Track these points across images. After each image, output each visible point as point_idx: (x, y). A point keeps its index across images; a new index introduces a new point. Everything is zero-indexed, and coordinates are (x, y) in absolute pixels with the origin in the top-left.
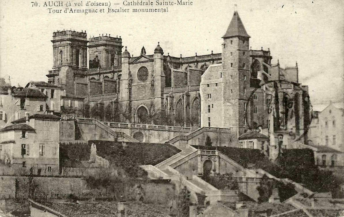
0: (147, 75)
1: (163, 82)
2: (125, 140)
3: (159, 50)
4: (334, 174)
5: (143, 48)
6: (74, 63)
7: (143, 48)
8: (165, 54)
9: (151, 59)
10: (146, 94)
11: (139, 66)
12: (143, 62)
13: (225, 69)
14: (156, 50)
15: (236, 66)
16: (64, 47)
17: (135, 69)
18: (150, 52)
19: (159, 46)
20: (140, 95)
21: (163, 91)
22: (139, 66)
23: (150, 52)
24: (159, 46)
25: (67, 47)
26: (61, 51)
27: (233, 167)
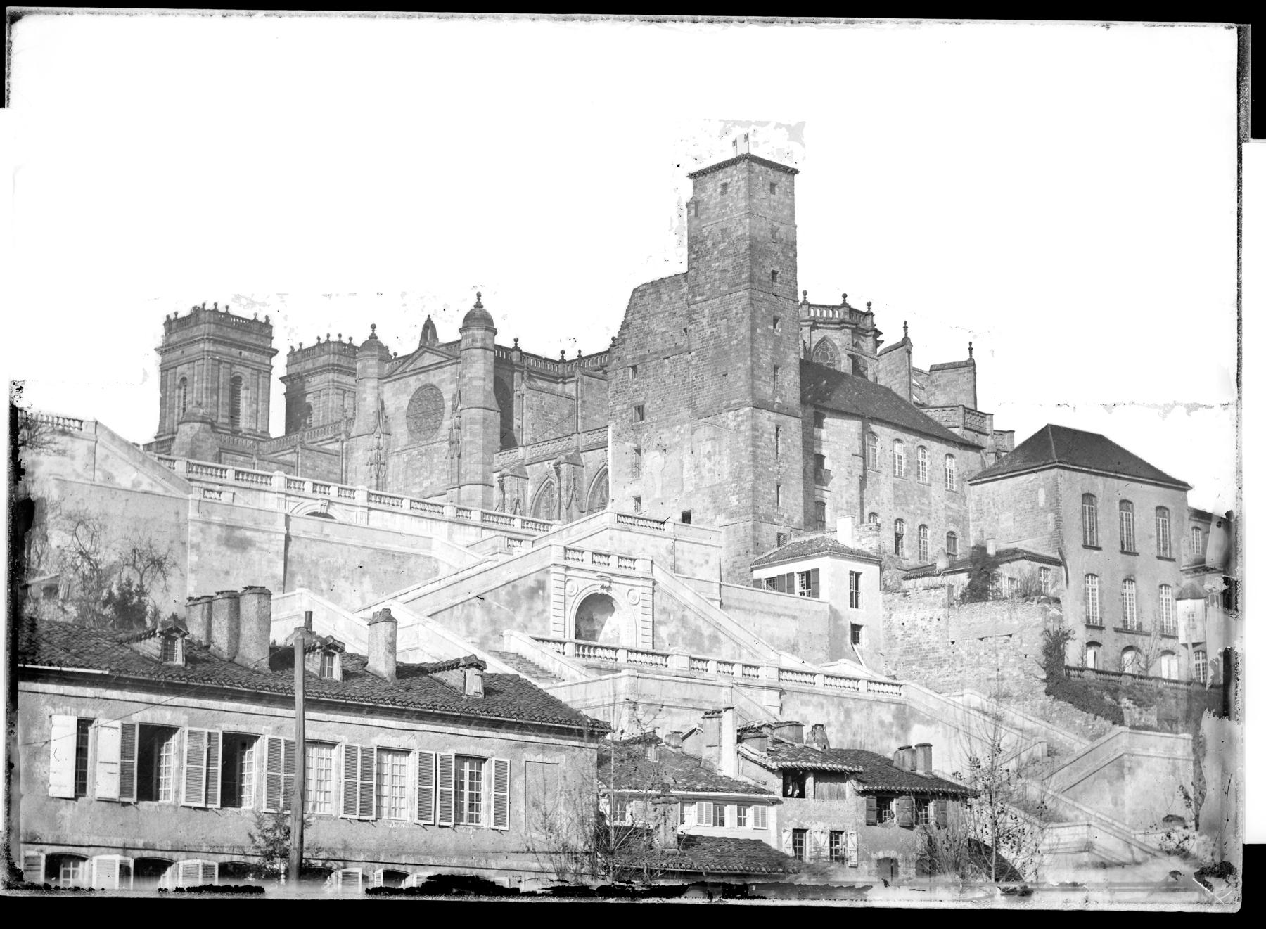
0: (439, 410)
1: (490, 431)
2: (1182, 735)
3: (478, 319)
4: (1044, 677)
5: (429, 321)
6: (223, 416)
7: (429, 321)
8: (504, 340)
9: (453, 352)
10: (434, 480)
11: (414, 383)
12: (425, 369)
13: (698, 299)
14: (468, 318)
15: (744, 276)
16: (191, 365)
17: (398, 398)
18: (448, 332)
19: (479, 306)
20: (415, 484)
21: (490, 464)
22: (414, 383)
23: (448, 332)
24: (479, 306)
25: (201, 362)
26: (184, 380)
27: (199, 524)
